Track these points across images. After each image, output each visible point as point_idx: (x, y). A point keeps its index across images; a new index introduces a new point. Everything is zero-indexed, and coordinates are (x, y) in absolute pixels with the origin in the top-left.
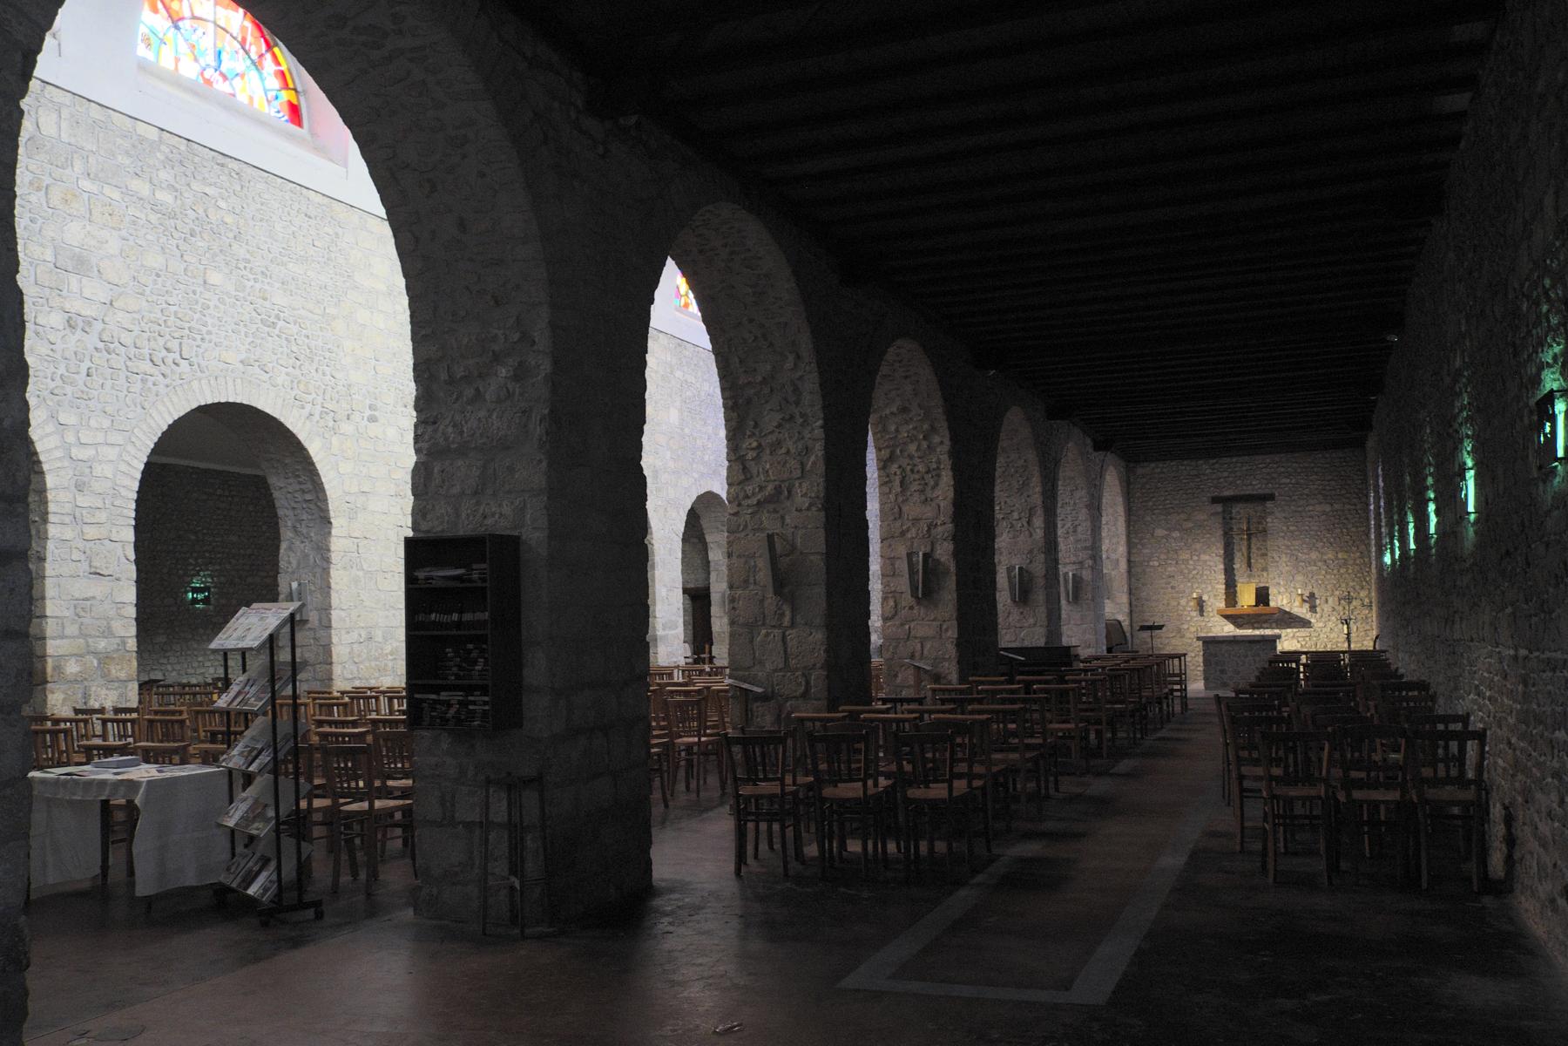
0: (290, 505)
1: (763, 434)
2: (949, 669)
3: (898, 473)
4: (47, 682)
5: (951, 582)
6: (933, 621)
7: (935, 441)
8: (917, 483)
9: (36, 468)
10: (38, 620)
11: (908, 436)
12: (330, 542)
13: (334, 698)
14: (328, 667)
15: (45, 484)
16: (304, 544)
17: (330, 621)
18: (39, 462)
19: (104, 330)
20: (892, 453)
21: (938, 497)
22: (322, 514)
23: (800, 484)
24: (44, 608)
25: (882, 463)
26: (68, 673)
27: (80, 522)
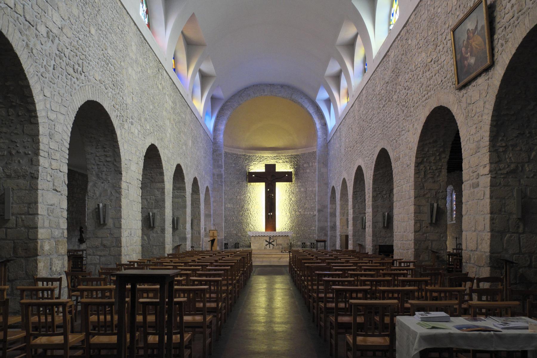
0: (96, 162)
1: (508, 140)
2: (443, 254)
3: (423, 169)
4: (37, 255)
6: (437, 233)
7: (443, 156)
8: (431, 174)
9: (32, 120)
11: (432, 153)
12: (121, 184)
14: (119, 249)
15: (39, 131)
16: (104, 184)
17: (121, 225)
18: (36, 117)
19: (59, 44)
20: (423, 160)
22: (116, 169)
23: (528, 165)
24: (37, 209)
25: (417, 164)
26: (45, 250)
27: (50, 158)
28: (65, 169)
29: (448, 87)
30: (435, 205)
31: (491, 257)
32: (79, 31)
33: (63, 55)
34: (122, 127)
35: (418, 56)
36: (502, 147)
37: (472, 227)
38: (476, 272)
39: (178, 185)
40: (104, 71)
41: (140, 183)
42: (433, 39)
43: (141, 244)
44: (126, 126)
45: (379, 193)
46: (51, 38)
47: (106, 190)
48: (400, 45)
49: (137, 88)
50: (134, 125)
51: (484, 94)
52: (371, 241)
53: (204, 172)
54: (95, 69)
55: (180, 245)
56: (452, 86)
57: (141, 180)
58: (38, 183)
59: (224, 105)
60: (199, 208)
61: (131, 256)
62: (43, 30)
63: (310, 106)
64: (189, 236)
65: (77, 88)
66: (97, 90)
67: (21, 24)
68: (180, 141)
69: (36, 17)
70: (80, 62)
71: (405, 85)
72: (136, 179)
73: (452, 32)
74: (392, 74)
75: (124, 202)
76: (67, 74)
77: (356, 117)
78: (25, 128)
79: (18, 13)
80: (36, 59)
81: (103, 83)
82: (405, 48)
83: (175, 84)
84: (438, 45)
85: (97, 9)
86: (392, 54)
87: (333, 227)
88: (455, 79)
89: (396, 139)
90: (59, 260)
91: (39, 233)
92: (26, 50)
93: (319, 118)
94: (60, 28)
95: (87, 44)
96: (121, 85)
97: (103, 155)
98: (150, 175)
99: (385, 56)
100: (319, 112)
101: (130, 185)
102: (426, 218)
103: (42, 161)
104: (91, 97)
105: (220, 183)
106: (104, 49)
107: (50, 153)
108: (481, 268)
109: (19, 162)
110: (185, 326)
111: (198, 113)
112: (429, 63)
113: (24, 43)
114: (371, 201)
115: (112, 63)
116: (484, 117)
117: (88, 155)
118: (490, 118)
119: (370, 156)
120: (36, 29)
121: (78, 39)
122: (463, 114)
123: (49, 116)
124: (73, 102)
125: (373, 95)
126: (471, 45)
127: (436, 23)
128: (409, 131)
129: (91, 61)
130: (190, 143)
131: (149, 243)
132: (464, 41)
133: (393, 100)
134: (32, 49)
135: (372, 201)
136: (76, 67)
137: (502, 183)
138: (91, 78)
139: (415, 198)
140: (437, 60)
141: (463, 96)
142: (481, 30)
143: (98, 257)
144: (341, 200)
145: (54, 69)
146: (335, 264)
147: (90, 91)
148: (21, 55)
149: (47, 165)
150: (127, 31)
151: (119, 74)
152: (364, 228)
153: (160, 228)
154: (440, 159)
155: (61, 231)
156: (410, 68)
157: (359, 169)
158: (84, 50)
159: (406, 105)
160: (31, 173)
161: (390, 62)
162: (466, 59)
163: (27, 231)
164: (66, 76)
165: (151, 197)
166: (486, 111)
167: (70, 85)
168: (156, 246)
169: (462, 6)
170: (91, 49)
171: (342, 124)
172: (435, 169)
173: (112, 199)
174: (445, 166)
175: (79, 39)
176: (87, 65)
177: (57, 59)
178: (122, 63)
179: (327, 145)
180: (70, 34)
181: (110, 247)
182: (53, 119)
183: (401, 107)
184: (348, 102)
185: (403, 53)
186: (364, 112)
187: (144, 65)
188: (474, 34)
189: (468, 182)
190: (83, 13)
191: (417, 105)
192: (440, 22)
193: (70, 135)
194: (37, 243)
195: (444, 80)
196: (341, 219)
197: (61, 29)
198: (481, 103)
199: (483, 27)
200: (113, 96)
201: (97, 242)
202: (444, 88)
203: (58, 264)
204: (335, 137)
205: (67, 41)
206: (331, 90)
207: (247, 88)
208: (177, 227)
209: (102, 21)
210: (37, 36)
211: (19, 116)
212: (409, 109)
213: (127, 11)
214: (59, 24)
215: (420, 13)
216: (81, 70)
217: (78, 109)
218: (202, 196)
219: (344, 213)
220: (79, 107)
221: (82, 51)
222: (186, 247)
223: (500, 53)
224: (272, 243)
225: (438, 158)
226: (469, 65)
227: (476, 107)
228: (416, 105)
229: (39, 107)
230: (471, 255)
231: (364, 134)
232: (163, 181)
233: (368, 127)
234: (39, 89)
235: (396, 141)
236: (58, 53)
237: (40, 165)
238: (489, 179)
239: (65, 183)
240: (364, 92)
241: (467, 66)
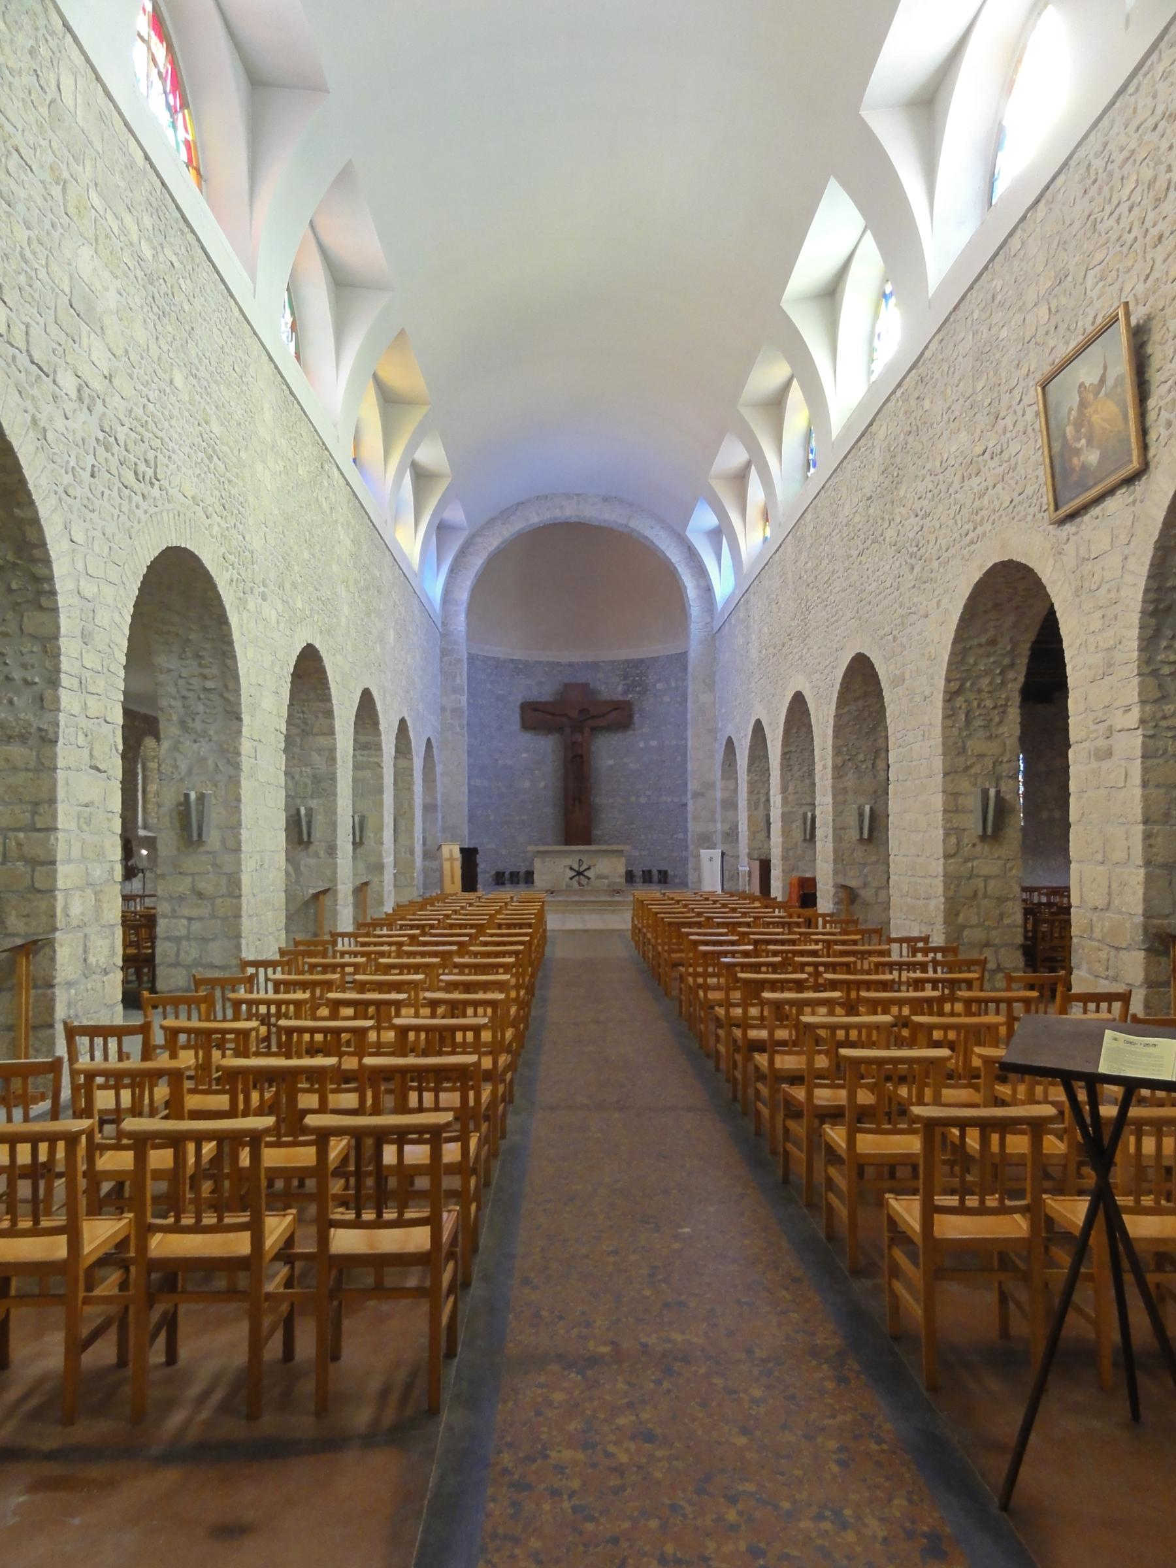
3: (963, 707)
5: (1020, 819)
8: (981, 718)
9: (44, 601)
10: (41, 835)
12: (240, 744)
13: (891, 966)
14: (235, 901)
15: (58, 628)
16: (197, 745)
17: (239, 843)
18: (53, 593)
19: (104, 414)
20: (962, 686)
21: (1003, 734)
24: (54, 817)
28: (118, 717)
29: (1030, 518)
30: (992, 792)
31: (1146, 928)
32: (147, 382)
33: (112, 440)
34: (241, 608)
35: (950, 439)
36: (1170, 663)
37: (1097, 852)
38: (1108, 960)
39: (363, 739)
40: (203, 475)
41: (282, 738)
42: (988, 401)
43: (283, 887)
44: (251, 605)
45: (847, 758)
46: (87, 401)
47: (202, 760)
48: (902, 410)
49: (276, 512)
50: (269, 600)
51: (1123, 538)
52: (831, 873)
53: (421, 704)
54: (184, 469)
55: (366, 884)
56: (1039, 516)
57: (285, 732)
58: (56, 754)
60: (410, 789)
61: (263, 917)
62: (68, 383)
64: (389, 860)
65: (144, 518)
66: (187, 521)
67: (20, 371)
68: (370, 633)
70: (151, 455)
71: (918, 505)
72: (273, 730)
73: (1039, 389)
74: (881, 479)
75: (247, 787)
76: (121, 485)
77: (790, 576)
78: (25, 619)
79: (16, 345)
80: (54, 453)
81: (201, 503)
82: (915, 419)
83: (357, 498)
84: (1001, 415)
85: (188, 328)
86: (881, 431)
87: (728, 834)
88: (1047, 498)
89: (894, 632)
90: (103, 938)
92: (31, 434)
93: (693, 575)
94: (106, 377)
95: (166, 412)
96: (240, 507)
97: (196, 674)
98: (301, 716)
99: (863, 435)
101: (260, 747)
102: (972, 823)
103: (65, 697)
104: (174, 540)
105: (458, 729)
106: (203, 423)
107: (83, 678)
108: (1122, 952)
109: (11, 702)
111: (409, 565)
112: (979, 456)
113: (28, 417)
114: (830, 776)
115: (221, 455)
116: (1123, 593)
117: (162, 673)
118: (1140, 596)
119: (826, 671)
120: (54, 382)
121: (145, 401)
122: (1070, 583)
123: (81, 588)
125: (832, 527)
126: (1089, 421)
127: (994, 363)
128: (927, 616)
129: (174, 451)
130: (391, 636)
132: (1071, 410)
133: (884, 540)
134: (45, 430)
135: (833, 778)
136: (142, 467)
137: (1170, 749)
138: (174, 492)
139: (945, 775)
140: (999, 450)
141: (1068, 539)
142: (1115, 386)
143: (185, 922)
144: (749, 771)
145: (93, 476)
146: (783, 945)
147: (172, 523)
148: (20, 447)
149: (76, 709)
150: (254, 376)
151: (235, 480)
152: (811, 837)
154: (1003, 683)
155: (107, 867)
156: (928, 466)
157: (799, 700)
158: (159, 426)
159: (919, 553)
160: (40, 729)
161: (877, 451)
162: (1077, 452)
163: (29, 869)
164: (119, 489)
165: (304, 769)
166: (1128, 578)
167: (127, 512)
169: (1062, 327)
170: (173, 422)
171: (752, 590)
172: (991, 706)
173: (219, 781)
174: (1016, 698)
175: (149, 401)
176: (166, 461)
177: (101, 450)
178: (243, 454)
179: (714, 638)
180: (128, 391)
181: (215, 898)
182: (88, 595)
183: (907, 558)
184: (765, 539)
185: (909, 428)
186: (810, 564)
187: (290, 455)
188: (1097, 394)
189: (1085, 745)
190: (157, 339)
191: (949, 554)
192: (1004, 362)
193: (127, 632)
194: (55, 898)
195: (1017, 500)
196: (750, 817)
197: (109, 378)
198: (1115, 560)
199: (1119, 381)
200: (222, 535)
201: (183, 886)
202: (1017, 518)
203: (101, 947)
204: (733, 621)
205: (122, 406)
206: (724, 507)
207: (523, 503)
208: (361, 838)
209: (198, 355)
210: (55, 398)
211: (10, 590)
212: (927, 563)
213: (252, 329)
214: (104, 367)
215: (954, 338)
216: (153, 475)
217: (145, 569)
218: (418, 762)
219: (759, 799)
220: (149, 564)
221: (155, 430)
222: (382, 887)
223: (1163, 443)
224: (585, 873)
225: (999, 681)
226: (1085, 467)
227: (1103, 569)
228: (945, 555)
229: (61, 568)
230: (1095, 919)
231: (810, 617)
232: (331, 732)
233: (820, 600)
234: (61, 526)
235: (895, 639)
236: (101, 435)
237: (62, 708)
238: (1140, 740)
239: (117, 750)
240: (808, 517)
241: (1077, 469)
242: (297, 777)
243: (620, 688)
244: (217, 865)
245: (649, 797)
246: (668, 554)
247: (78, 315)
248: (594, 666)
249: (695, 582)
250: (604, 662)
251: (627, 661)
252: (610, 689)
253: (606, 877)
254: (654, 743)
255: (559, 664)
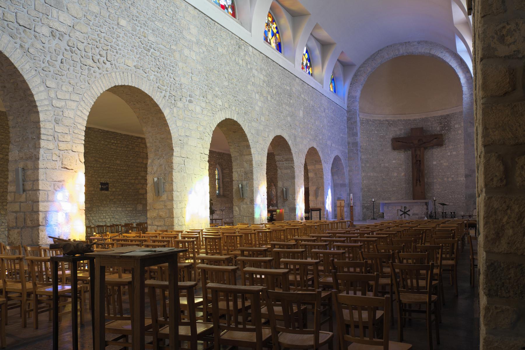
10: (34, 192)
12: (173, 159)
14: (171, 219)
16: (160, 160)
17: (172, 197)
19: (69, 40)
24: (38, 185)
59: (357, 71)
63: (452, 59)
69: (34, 21)
79: (8, 20)
91: (40, 207)
100: (464, 65)
101: (186, 160)
105: (355, 152)
110: (347, 294)
120: (34, 31)
124: (91, 89)
131: (240, 214)
153: (249, 199)
160: (35, 155)
165: (241, 169)
168: (246, 216)
181: (165, 218)
208: (286, 198)
210: (35, 37)
242: (239, 172)
243: (438, 129)
244: (165, 206)
245: (453, 178)
246: (450, 64)
247: (51, 6)
248: (426, 120)
249: (464, 75)
250: (431, 117)
251: (441, 116)
252: (436, 128)
253: (417, 214)
254: (454, 153)
255: (409, 120)
